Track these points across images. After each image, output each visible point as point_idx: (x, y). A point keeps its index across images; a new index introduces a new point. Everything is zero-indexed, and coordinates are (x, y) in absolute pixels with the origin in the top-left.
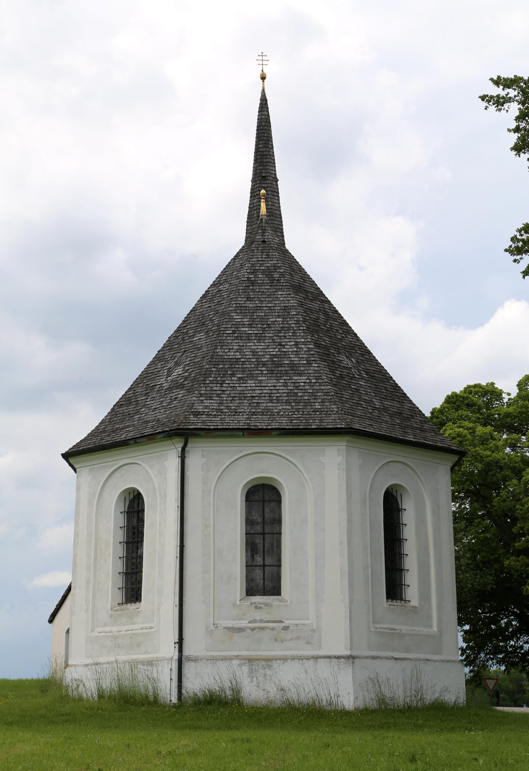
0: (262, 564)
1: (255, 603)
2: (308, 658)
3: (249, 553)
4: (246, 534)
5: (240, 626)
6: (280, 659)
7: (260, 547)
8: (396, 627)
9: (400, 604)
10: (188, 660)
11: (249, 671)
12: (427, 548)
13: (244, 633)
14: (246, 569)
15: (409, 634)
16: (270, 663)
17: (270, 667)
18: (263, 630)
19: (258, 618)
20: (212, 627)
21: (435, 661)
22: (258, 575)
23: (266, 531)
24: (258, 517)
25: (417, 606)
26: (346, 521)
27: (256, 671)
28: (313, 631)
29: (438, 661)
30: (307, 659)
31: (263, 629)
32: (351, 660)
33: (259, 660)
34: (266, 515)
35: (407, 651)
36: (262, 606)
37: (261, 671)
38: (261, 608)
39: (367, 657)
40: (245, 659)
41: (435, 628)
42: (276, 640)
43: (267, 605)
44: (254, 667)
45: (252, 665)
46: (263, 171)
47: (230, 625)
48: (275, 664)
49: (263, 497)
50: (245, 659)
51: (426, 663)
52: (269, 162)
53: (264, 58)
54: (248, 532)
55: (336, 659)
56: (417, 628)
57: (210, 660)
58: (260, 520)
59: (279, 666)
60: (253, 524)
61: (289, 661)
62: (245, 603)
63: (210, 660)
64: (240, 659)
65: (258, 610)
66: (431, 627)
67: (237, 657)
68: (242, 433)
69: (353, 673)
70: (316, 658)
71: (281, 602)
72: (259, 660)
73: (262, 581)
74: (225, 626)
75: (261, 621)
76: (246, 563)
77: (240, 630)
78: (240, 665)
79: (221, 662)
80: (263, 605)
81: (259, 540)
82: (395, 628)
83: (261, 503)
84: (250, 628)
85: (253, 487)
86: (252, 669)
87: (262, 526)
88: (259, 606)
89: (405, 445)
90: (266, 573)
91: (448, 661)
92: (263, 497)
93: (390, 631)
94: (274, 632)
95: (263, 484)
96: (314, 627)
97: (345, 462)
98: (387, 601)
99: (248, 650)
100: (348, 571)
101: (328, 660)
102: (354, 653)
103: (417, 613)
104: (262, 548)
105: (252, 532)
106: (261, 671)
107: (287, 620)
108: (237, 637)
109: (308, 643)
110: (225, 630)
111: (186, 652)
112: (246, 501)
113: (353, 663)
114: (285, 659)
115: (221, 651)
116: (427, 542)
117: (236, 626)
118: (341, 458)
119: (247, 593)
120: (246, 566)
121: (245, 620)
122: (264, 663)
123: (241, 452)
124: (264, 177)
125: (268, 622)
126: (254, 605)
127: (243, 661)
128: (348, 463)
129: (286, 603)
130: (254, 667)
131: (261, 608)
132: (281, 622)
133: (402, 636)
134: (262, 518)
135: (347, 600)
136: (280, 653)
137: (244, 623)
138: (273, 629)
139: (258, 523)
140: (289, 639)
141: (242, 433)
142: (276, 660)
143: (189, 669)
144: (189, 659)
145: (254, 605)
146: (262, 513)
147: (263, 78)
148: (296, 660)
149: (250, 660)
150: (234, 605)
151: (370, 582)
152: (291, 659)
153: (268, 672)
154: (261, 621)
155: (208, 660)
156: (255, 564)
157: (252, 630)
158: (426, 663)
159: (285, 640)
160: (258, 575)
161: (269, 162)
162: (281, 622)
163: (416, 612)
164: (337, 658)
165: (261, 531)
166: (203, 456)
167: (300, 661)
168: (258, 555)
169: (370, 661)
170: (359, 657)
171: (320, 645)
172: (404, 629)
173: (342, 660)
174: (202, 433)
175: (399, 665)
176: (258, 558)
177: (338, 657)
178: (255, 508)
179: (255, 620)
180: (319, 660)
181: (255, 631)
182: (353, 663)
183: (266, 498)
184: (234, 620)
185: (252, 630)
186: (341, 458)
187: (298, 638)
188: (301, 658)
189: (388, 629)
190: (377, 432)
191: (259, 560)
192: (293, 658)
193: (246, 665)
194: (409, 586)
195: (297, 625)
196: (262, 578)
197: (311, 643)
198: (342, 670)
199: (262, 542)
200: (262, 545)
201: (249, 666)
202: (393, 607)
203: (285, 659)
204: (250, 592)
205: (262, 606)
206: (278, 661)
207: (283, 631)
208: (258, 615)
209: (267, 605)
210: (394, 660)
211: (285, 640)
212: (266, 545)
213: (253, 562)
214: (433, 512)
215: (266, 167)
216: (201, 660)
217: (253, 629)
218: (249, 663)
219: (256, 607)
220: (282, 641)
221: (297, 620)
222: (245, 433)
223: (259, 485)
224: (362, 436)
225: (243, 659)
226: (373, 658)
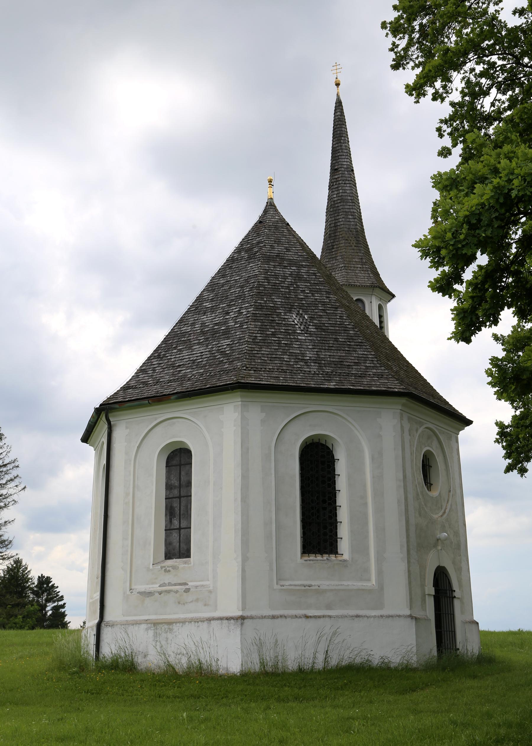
0: (178, 527)
1: (165, 567)
2: (202, 620)
3: (168, 517)
4: (166, 499)
5: (152, 590)
6: (179, 622)
7: (177, 510)
8: (313, 583)
9: (321, 558)
10: (107, 626)
11: (154, 635)
12: (364, 497)
13: (153, 597)
14: (166, 533)
15: (332, 590)
16: (171, 627)
17: (171, 630)
18: (169, 593)
19: (167, 582)
20: (128, 593)
21: (368, 617)
22: (175, 538)
23: (182, 494)
24: (176, 482)
25: (348, 559)
26: (240, 478)
27: (160, 634)
28: (210, 592)
29: (375, 617)
30: (202, 621)
31: (168, 592)
32: (240, 621)
33: (162, 623)
34: (182, 478)
35: (329, 607)
36: (170, 569)
37: (164, 635)
38: (169, 571)
39: (263, 617)
40: (151, 623)
41: (374, 582)
42: (179, 603)
43: (174, 568)
44: (158, 631)
45: (157, 629)
46: (336, 164)
47: (143, 590)
48: (175, 627)
49: (180, 461)
50: (151, 623)
51: (353, 619)
52: (341, 155)
53: (338, 67)
54: (167, 497)
55: (227, 621)
56: (345, 583)
57: (123, 625)
58: (177, 484)
59: (178, 629)
60: (171, 489)
61: (187, 623)
62: (157, 567)
63: (123, 625)
64: (147, 624)
65: (167, 573)
66: (369, 580)
67: (146, 621)
68: (147, 402)
69: (241, 634)
70: (210, 620)
71: (185, 564)
72: (162, 623)
73: (178, 544)
74: (138, 591)
75: (170, 584)
76: (166, 527)
77: (150, 594)
78: (147, 629)
79: (132, 626)
80: (171, 568)
81: (176, 504)
82: (313, 584)
83: (178, 467)
84: (158, 592)
85: (172, 452)
86: (156, 633)
87: (179, 490)
88: (168, 569)
89: (353, 394)
90: (182, 536)
91: (389, 617)
92: (180, 461)
93: (303, 588)
94: (178, 595)
95: (181, 449)
96: (211, 588)
97: (240, 417)
98: (302, 557)
99: (156, 614)
100: (242, 528)
101: (220, 621)
102: (245, 615)
103: (347, 566)
104: (178, 512)
105: (171, 496)
106: (164, 635)
107: (191, 582)
108: (148, 601)
109: (205, 605)
110: (139, 595)
111: (108, 617)
112: (166, 467)
113: (242, 624)
114: (183, 622)
115: (135, 615)
116: (365, 491)
117: (147, 591)
118: (237, 414)
119: (165, 557)
120: (165, 530)
121: (156, 584)
122: (166, 626)
123: (156, 419)
124: (336, 169)
125: (175, 585)
126: (164, 569)
127: (149, 625)
128: (243, 418)
129: (190, 565)
130: (158, 631)
131: (169, 571)
132: (185, 584)
133: (320, 592)
134: (179, 482)
135: (240, 559)
136: (182, 616)
137: (156, 587)
138: (177, 592)
139: (175, 487)
140: (190, 601)
141: (147, 402)
142: (176, 623)
143: (107, 634)
144: (112, 625)
145: (164, 569)
146: (179, 478)
147: (338, 85)
148: (192, 622)
149: (156, 624)
150: (148, 569)
151: (274, 538)
152: (189, 622)
153: (170, 636)
154: (170, 584)
155: (121, 625)
156: (172, 527)
157: (160, 594)
158: (353, 619)
159: (186, 603)
160: (175, 538)
161: (341, 155)
162: (185, 584)
163: (346, 566)
164: (228, 620)
165: (178, 495)
166: (127, 428)
167: (196, 623)
168: (175, 519)
169: (270, 621)
170: (252, 618)
171: (216, 606)
172: (325, 584)
173: (232, 621)
174: (117, 406)
175: (311, 624)
176: (175, 521)
177: (228, 619)
178: (173, 472)
179: (164, 583)
180: (212, 622)
181: (162, 595)
182: (242, 624)
183: (183, 463)
184: (147, 584)
185: (160, 594)
186: (237, 414)
187: (197, 600)
188: (197, 621)
189: (301, 585)
190: (291, 384)
191: (176, 522)
192: (191, 621)
193: (152, 629)
194: (342, 538)
195: (196, 587)
196: (178, 541)
197: (208, 605)
198: (231, 632)
199: (178, 505)
200: (178, 508)
201: (154, 630)
202: (311, 562)
203: (183, 622)
204: (168, 556)
205: (170, 569)
206: (178, 624)
207: (185, 594)
208: (168, 578)
209: (174, 568)
210: (304, 619)
211: (186, 603)
212: (182, 508)
213: (171, 526)
214: (373, 459)
215: (338, 161)
216: (117, 625)
217: (160, 593)
218: (154, 627)
219: (166, 571)
220: (184, 604)
221: (199, 581)
222: (150, 401)
223: (177, 450)
224: (251, 389)
225: (149, 623)
226: (273, 617)
